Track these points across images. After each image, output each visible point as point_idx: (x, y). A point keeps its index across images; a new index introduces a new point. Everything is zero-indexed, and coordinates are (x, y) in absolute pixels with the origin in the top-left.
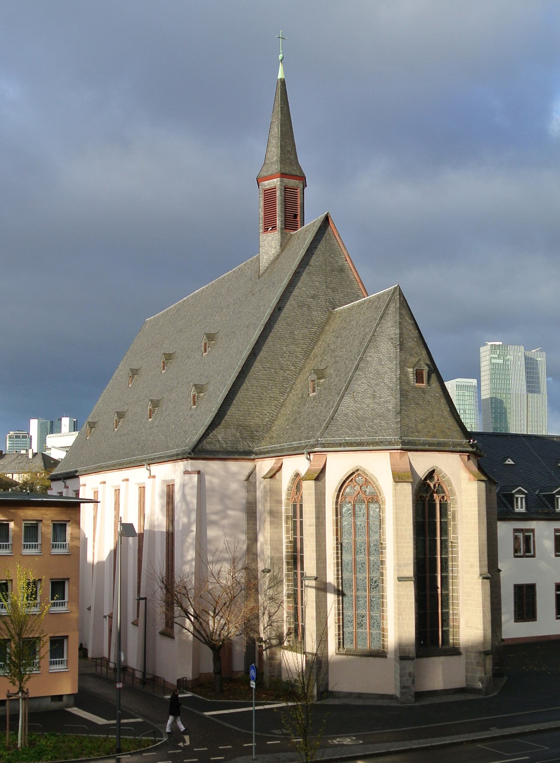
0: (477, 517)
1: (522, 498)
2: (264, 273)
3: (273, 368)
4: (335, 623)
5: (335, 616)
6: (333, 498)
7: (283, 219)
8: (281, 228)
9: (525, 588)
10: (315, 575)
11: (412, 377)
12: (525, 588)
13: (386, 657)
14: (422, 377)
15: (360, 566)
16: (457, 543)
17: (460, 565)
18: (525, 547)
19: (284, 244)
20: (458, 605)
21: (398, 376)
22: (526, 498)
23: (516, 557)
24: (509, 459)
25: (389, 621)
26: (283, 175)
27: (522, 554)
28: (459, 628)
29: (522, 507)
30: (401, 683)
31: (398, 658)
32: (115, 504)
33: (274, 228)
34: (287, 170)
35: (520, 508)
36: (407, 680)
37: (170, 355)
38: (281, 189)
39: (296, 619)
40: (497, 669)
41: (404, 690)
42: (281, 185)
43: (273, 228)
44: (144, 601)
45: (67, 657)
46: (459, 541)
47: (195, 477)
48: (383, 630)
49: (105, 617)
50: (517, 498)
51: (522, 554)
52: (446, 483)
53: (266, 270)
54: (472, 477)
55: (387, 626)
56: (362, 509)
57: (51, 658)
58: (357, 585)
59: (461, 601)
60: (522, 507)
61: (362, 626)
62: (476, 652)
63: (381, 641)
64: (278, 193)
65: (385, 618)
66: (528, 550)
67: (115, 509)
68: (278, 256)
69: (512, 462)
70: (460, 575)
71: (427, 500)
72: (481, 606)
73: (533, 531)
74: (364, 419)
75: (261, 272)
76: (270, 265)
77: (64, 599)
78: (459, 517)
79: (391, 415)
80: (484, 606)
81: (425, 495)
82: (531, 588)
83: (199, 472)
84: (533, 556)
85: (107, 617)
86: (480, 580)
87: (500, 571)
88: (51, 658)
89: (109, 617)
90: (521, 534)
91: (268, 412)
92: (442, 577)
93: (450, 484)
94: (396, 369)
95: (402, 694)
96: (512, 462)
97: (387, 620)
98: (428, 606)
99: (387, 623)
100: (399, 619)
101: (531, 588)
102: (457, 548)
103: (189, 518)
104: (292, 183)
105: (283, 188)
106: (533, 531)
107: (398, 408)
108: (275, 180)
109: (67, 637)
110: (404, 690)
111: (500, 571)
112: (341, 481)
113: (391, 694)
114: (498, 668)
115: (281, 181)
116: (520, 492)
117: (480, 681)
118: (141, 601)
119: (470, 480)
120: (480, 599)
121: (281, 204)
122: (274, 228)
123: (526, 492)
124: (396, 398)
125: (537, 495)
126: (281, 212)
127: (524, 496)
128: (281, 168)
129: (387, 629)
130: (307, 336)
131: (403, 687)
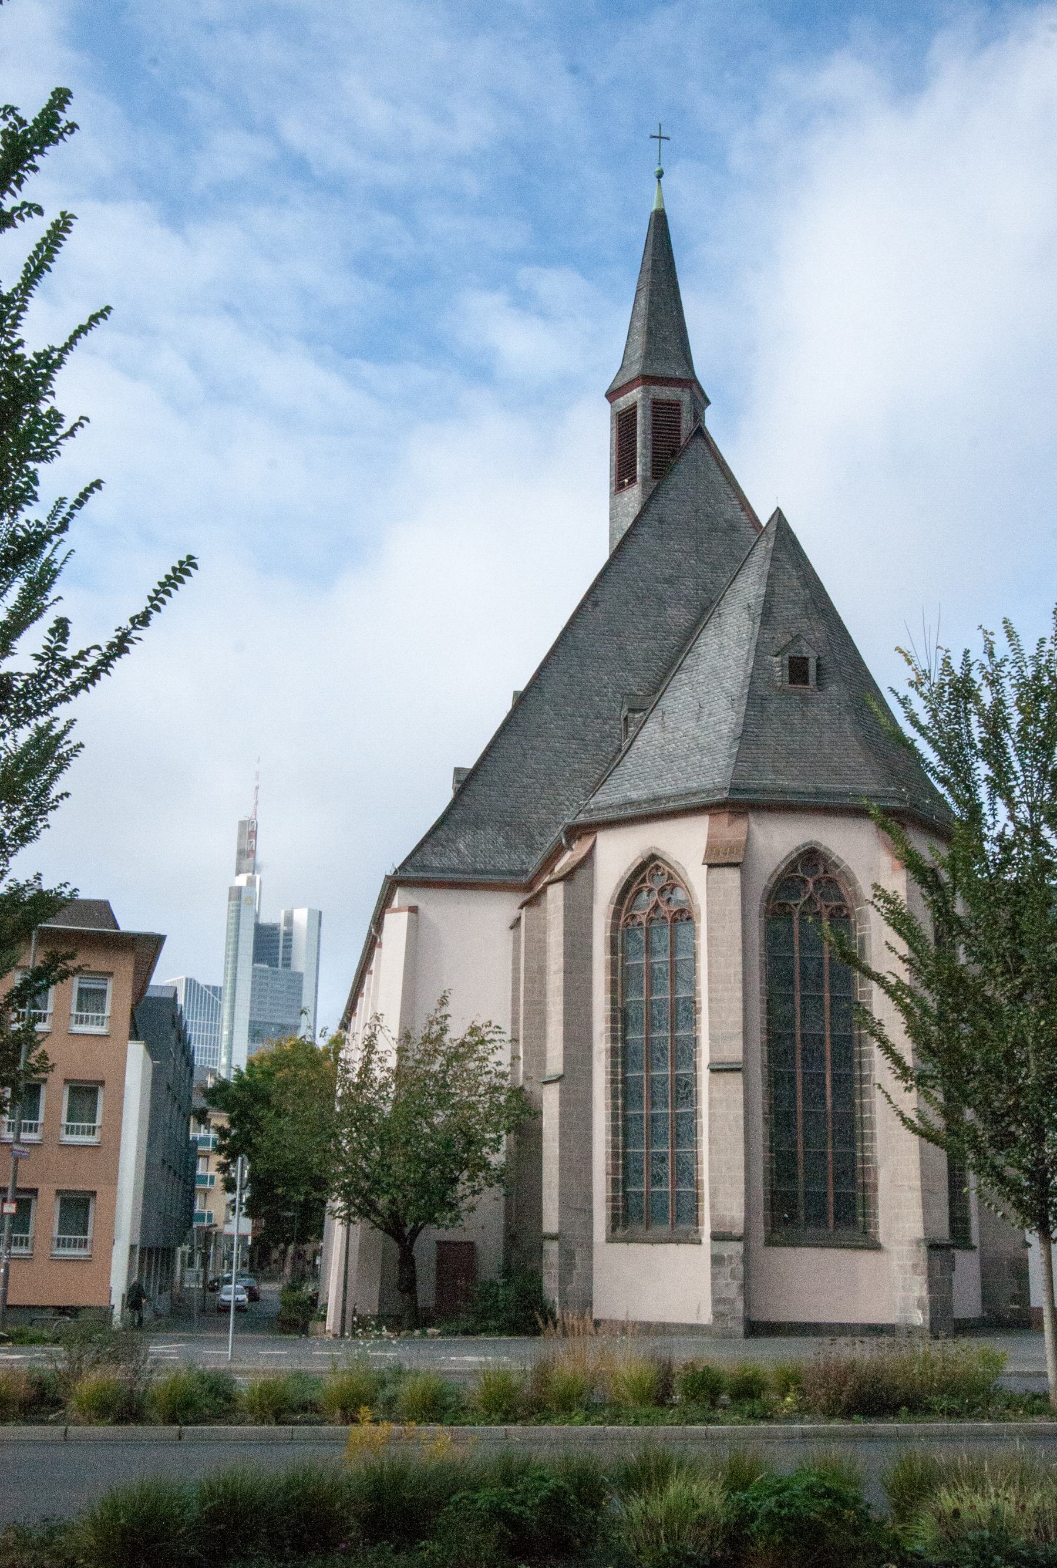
3: (581, 716)
4: (607, 1174)
5: (607, 1159)
6: (607, 917)
7: (649, 459)
8: (645, 479)
10: (561, 1072)
14: (806, 673)
15: (659, 1054)
20: (872, 1138)
21: (750, 671)
26: (646, 380)
28: (876, 1190)
34: (661, 369)
36: (727, 1285)
41: (721, 1308)
58: (653, 1094)
59: (878, 1131)
62: (911, 1242)
64: (639, 412)
71: (797, 910)
77: (94, 1122)
79: (723, 745)
81: (792, 903)
88: (60, 1233)
91: (568, 799)
92: (836, 1079)
94: (748, 659)
95: (718, 1315)
103: (21, 818)
104: (666, 393)
107: (739, 731)
109: (94, 1194)
110: (721, 1308)
112: (621, 881)
114: (1017, 1307)
115: (646, 392)
117: (919, 1307)
119: (893, 869)
124: (737, 713)
128: (644, 367)
130: (654, 654)
131: (717, 1301)
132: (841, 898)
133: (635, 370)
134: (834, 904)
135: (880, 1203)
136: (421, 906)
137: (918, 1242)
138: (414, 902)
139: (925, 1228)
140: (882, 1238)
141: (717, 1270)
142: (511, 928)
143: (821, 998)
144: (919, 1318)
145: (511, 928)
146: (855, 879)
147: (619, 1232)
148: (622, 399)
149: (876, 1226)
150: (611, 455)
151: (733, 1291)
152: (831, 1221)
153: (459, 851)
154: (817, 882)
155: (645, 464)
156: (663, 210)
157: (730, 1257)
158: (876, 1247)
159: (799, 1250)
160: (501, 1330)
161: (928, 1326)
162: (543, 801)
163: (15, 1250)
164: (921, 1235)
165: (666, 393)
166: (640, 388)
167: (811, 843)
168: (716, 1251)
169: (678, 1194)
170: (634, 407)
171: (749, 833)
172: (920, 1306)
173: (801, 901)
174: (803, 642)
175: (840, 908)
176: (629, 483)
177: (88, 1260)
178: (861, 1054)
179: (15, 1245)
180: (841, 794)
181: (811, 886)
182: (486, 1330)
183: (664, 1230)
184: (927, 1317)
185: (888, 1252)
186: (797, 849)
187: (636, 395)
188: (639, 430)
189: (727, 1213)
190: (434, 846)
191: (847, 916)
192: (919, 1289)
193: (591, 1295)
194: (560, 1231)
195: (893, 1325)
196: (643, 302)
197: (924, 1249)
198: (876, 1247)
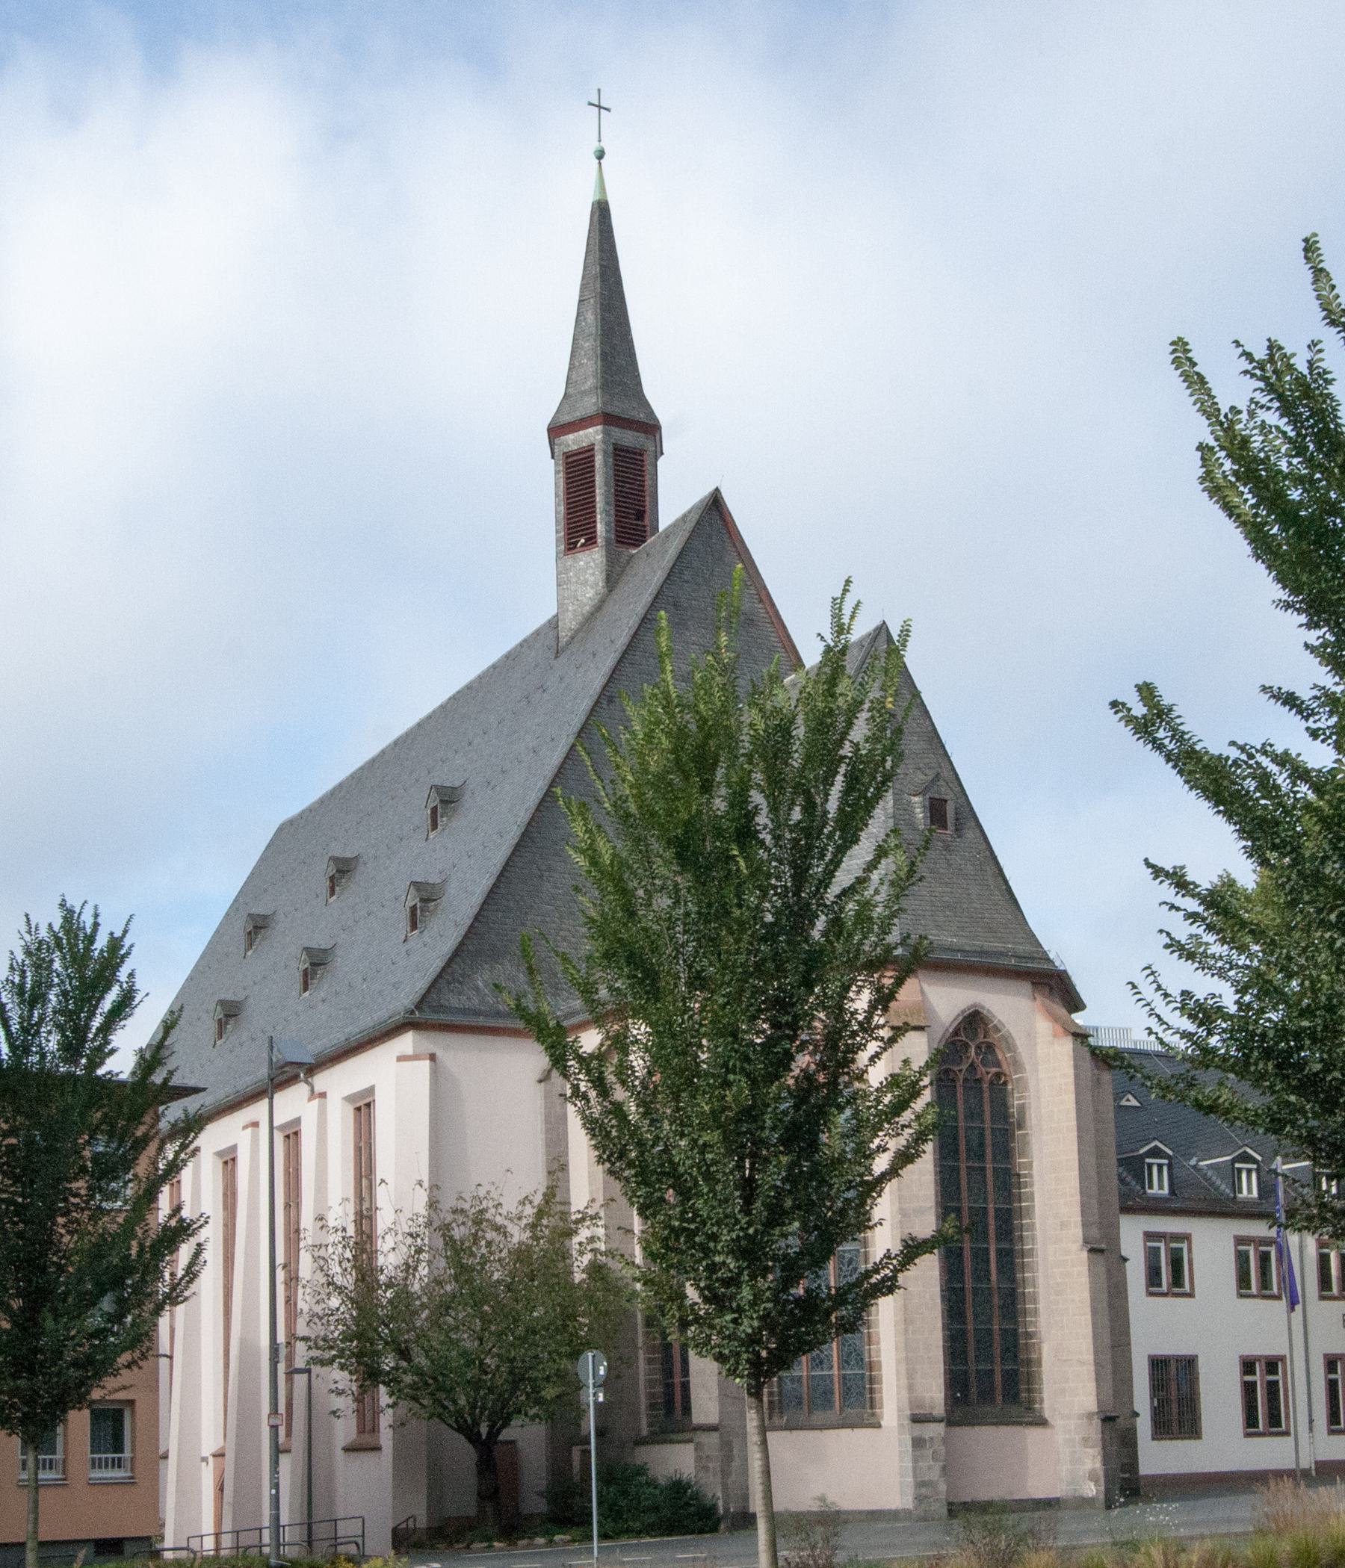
0: (1073, 1115)
1: (1160, 1166)
2: (568, 643)
7: (613, 519)
8: (608, 541)
11: (920, 814)
13: (880, 1426)
16: (1031, 1176)
17: (1038, 1226)
18: (1171, 1273)
19: (613, 579)
21: (891, 811)
22: (1170, 1166)
23: (1151, 1294)
24: (1130, 1097)
25: (883, 1345)
26: (608, 419)
27: (1164, 1288)
29: (1161, 1187)
30: (915, 1476)
31: (907, 1422)
32: (225, 1195)
33: (591, 541)
34: (618, 408)
35: (1159, 1187)
37: (347, 861)
38: (605, 452)
39: (668, 1373)
40: (1124, 1479)
42: (604, 442)
43: (587, 540)
44: (306, 1376)
45: (133, 1450)
46: (1035, 1171)
47: (426, 1064)
48: (871, 1366)
49: (204, 1459)
50: (1150, 1166)
52: (1004, 1045)
53: (572, 638)
55: (878, 1356)
57: (92, 1452)
59: (1041, 1306)
60: (1161, 1187)
61: (821, 1362)
62: (1081, 1417)
63: (867, 1392)
64: (599, 459)
65: (874, 1339)
66: (1177, 1279)
67: (225, 1208)
68: (602, 602)
69: (1134, 1103)
70: (1039, 1246)
71: (961, 1077)
72: (1088, 1310)
73: (1186, 1238)
75: (563, 641)
76: (582, 625)
78: (1032, 1118)
80: (1094, 1312)
81: (956, 1069)
82: (1189, 1364)
83: (432, 1057)
84: (1191, 1295)
85: (211, 1459)
86: (1085, 1254)
87: (1125, 1260)
88: (92, 1452)
89: (214, 1456)
90: (1162, 1245)
93: (1011, 1047)
95: (919, 1499)
96: (1134, 1103)
97: (878, 1343)
98: (970, 1316)
99: (878, 1351)
100: (906, 1330)
101: (1189, 1364)
102: (1032, 1186)
104: (629, 438)
105: (611, 447)
106: (1186, 1238)
108: (590, 430)
109: (131, 1403)
110: (924, 1491)
111: (1125, 1260)
113: (893, 1507)
115: (606, 433)
116: (1156, 1153)
118: (296, 1377)
119: (1055, 1036)
120: (1086, 1295)
121: (606, 484)
122: (591, 541)
123: (1171, 1153)
125: (1194, 1167)
126: (607, 503)
127: (1166, 1161)
128: (604, 403)
129: (879, 1362)
131: (920, 1484)
132: (998, 1064)
133: (591, 404)
134: (994, 1070)
135: (1045, 1377)
136: (439, 1054)
137: (1090, 1416)
138: (432, 1049)
139: (1099, 1401)
140: (1047, 1414)
141: (918, 1453)
142: (540, 1081)
143: (983, 1169)
144: (1091, 1490)
145: (540, 1081)
146: (1015, 1045)
147: (776, 1420)
148: (571, 436)
149: (1042, 1401)
150: (557, 505)
151: (935, 1474)
152: (999, 1398)
153: (477, 989)
154: (978, 1047)
155: (608, 524)
156: (607, 203)
157: (931, 1439)
158: (1043, 1423)
159: (977, 1428)
160: (650, 1530)
161: (1102, 1497)
162: (562, 933)
163: (42, 1475)
164: (1094, 1408)
165: (629, 438)
166: (599, 427)
167: (975, 1005)
168: (916, 1434)
169: (844, 1377)
170: (590, 449)
171: (922, 992)
172: (1092, 1477)
173: (964, 1067)
174: (942, 782)
175: (998, 1075)
176: (583, 545)
177: (130, 1482)
178: (1021, 1228)
179: (44, 1468)
180: (1002, 954)
181: (973, 1051)
182: (628, 1532)
183: (834, 1415)
184: (1102, 1488)
185: (1053, 1427)
186: (963, 1012)
187: (593, 435)
188: (599, 480)
189: (927, 1395)
190: (449, 983)
191: (1005, 1083)
192: (1092, 1460)
193: (747, 1488)
194: (721, 1421)
195: (1058, 1499)
196: (590, 317)
197: (1097, 1422)
198: (1043, 1423)
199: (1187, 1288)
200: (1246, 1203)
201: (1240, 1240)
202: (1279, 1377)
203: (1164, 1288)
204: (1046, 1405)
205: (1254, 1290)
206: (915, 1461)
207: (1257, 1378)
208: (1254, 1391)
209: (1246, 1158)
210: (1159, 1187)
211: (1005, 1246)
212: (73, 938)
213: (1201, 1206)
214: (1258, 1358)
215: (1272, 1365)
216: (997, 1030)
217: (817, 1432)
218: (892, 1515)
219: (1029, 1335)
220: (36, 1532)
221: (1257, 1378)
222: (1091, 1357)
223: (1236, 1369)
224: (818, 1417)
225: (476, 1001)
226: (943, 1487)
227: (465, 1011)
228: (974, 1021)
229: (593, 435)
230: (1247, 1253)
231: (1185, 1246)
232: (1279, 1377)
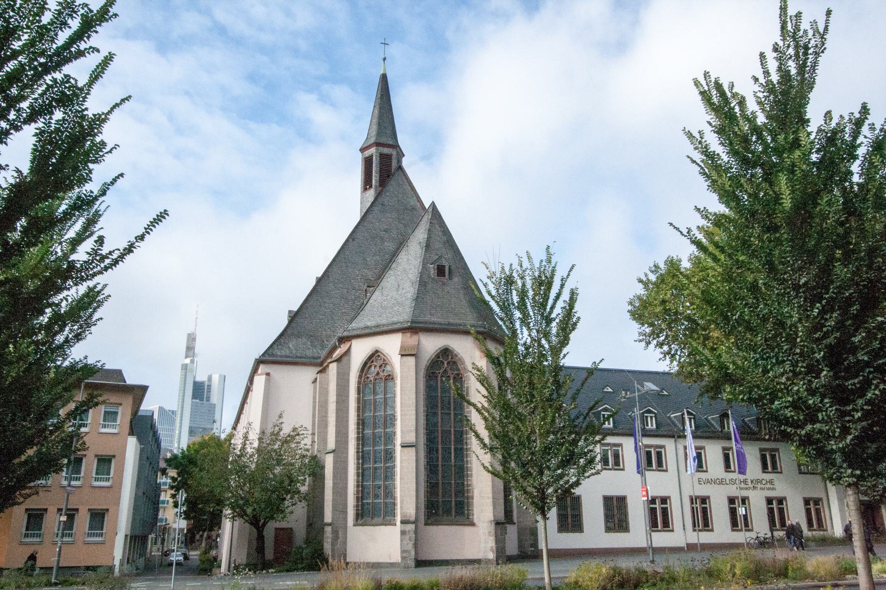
8: (376, 187)
9: (615, 500)
12: (615, 500)
14: (444, 273)
23: (733, 530)
26: (377, 144)
27: (610, 467)
29: (652, 425)
33: (371, 187)
34: (383, 140)
41: (404, 555)
51: (610, 467)
54: (482, 354)
56: (380, 388)
58: (375, 457)
69: (610, 390)
73: (620, 445)
74: (385, 308)
82: (622, 500)
83: (268, 374)
84: (623, 470)
95: (403, 558)
96: (610, 390)
101: (622, 500)
104: (386, 151)
107: (415, 296)
110: (404, 555)
115: (377, 150)
131: (403, 552)
132: (459, 370)
136: (271, 373)
137: (491, 521)
140: (475, 521)
144: (491, 556)
152: (453, 513)
153: (289, 348)
154: (448, 363)
158: (473, 524)
165: (386, 151)
175: (458, 375)
183: (380, 520)
187: (373, 151)
192: (491, 543)
198: (473, 524)
199: (621, 467)
200: (651, 430)
201: (761, 450)
202: (668, 506)
203: (654, 468)
204: (475, 517)
205: (770, 469)
206: (401, 541)
207: (657, 506)
208: (656, 512)
209: (649, 412)
210: (652, 425)
211: (459, 446)
212: (189, 335)
213: (628, 432)
214: (657, 497)
215: (664, 500)
216: (456, 356)
217: (372, 527)
218: (392, 565)
219: (468, 485)
220: (58, 561)
221: (657, 506)
222: (491, 495)
223: (802, 503)
224: (376, 520)
225: (288, 352)
226: (413, 553)
227: (281, 356)
228: (446, 352)
229: (373, 151)
230: (650, 452)
231: (620, 449)
232: (668, 506)
